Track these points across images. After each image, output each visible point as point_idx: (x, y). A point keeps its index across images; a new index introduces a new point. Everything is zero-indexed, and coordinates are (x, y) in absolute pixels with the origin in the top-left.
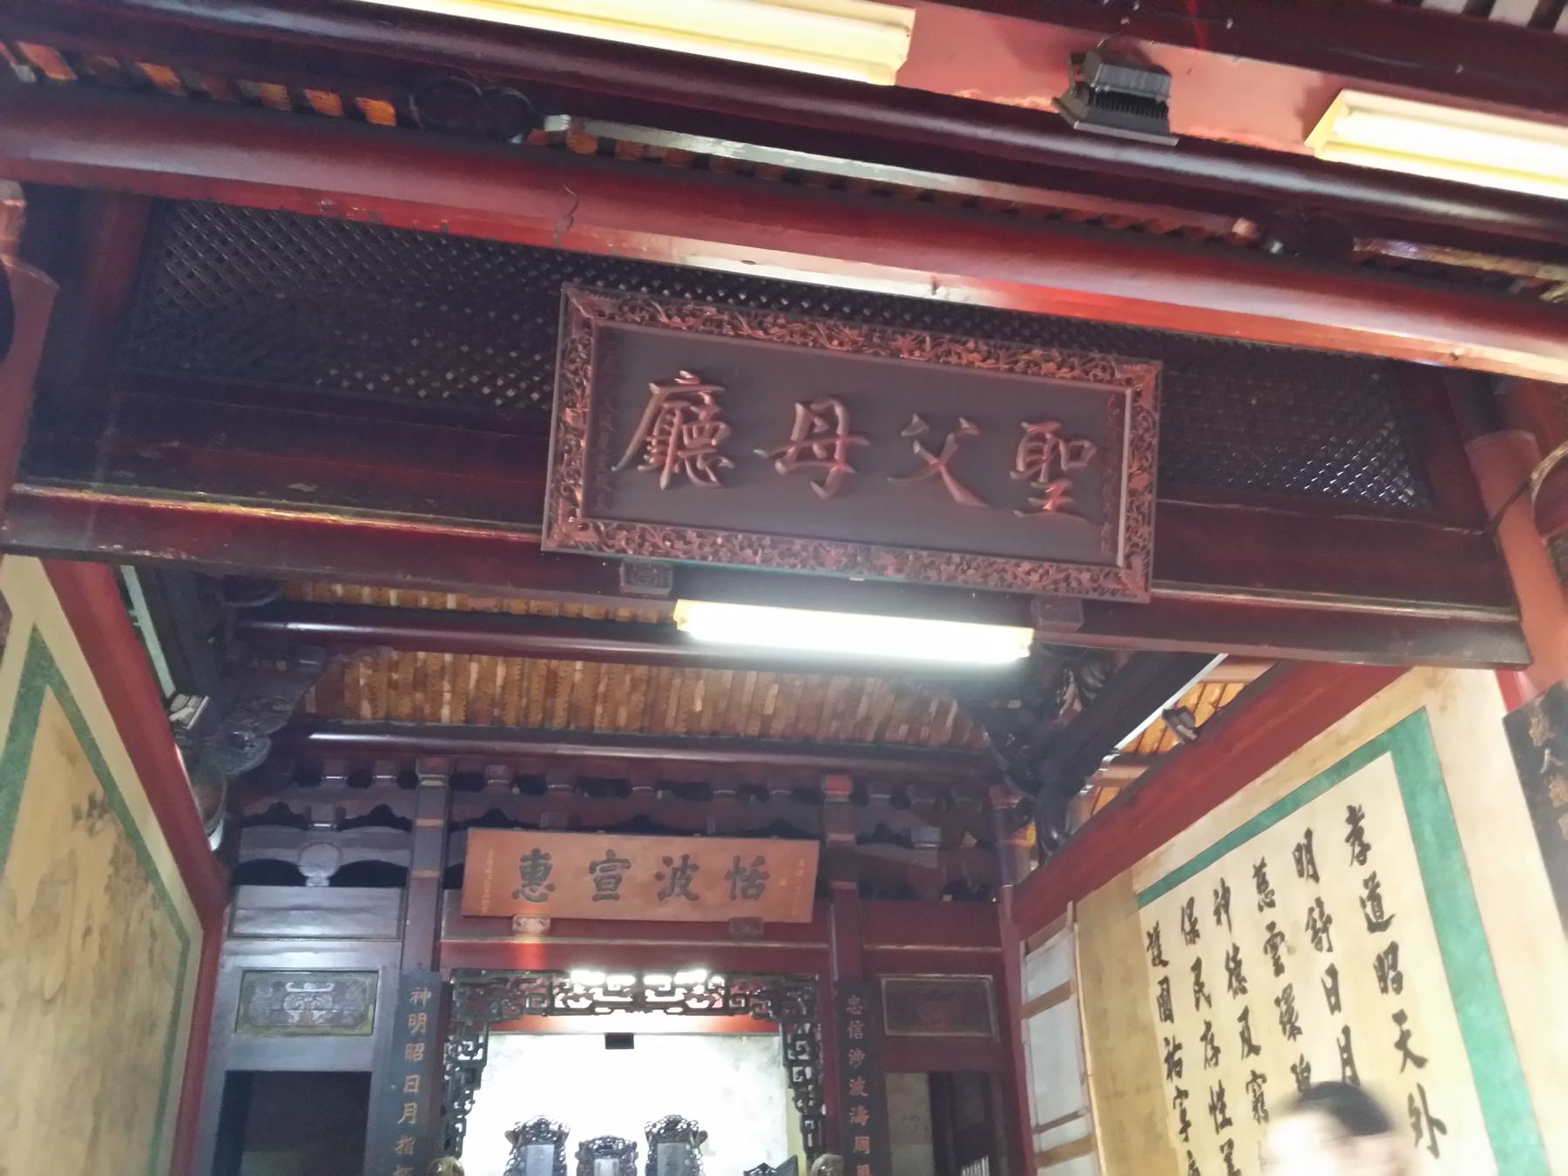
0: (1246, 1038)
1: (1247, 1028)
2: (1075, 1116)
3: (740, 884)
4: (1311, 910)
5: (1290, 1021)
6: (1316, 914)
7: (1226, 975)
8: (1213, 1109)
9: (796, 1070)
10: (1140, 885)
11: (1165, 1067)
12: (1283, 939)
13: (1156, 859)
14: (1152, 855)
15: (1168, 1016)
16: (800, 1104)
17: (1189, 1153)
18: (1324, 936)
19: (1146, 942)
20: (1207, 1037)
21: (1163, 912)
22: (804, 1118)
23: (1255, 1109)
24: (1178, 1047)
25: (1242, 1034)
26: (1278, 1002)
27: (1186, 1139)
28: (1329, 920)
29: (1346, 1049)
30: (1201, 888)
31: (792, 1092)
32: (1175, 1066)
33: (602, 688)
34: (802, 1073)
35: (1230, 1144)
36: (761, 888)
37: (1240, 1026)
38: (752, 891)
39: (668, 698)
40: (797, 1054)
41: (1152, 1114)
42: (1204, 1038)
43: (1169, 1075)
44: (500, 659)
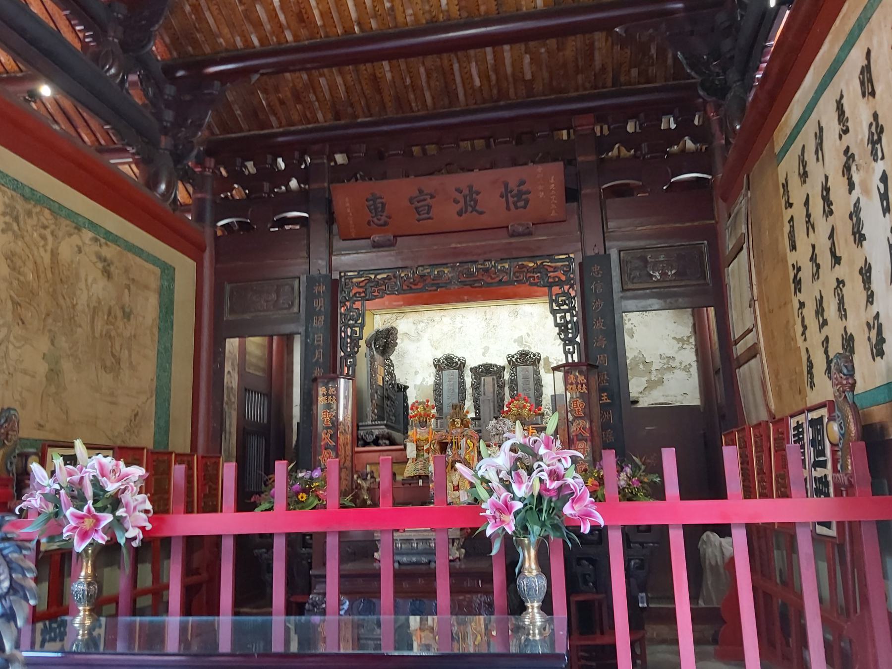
0: (833, 253)
1: (833, 243)
2: (750, 331)
3: (511, 200)
4: (871, 125)
5: (859, 232)
6: (873, 129)
7: (822, 202)
8: (817, 313)
9: (558, 315)
10: (777, 150)
11: (793, 286)
12: (854, 160)
13: (786, 121)
14: (783, 119)
15: (794, 247)
16: (562, 336)
17: (807, 349)
18: (878, 146)
19: (782, 190)
20: (813, 258)
21: (788, 166)
22: (565, 345)
23: (839, 310)
24: (799, 269)
25: (831, 249)
26: (851, 217)
27: (805, 340)
28: (882, 131)
29: (831, 237)
30: (807, 136)
31: (557, 330)
32: (798, 282)
33: (408, 81)
34: (564, 317)
35: (827, 339)
36: (527, 202)
37: (829, 243)
38: (521, 204)
39: (454, 80)
40: (559, 305)
41: (788, 322)
42: (811, 259)
43: (795, 293)
44: (334, 70)
